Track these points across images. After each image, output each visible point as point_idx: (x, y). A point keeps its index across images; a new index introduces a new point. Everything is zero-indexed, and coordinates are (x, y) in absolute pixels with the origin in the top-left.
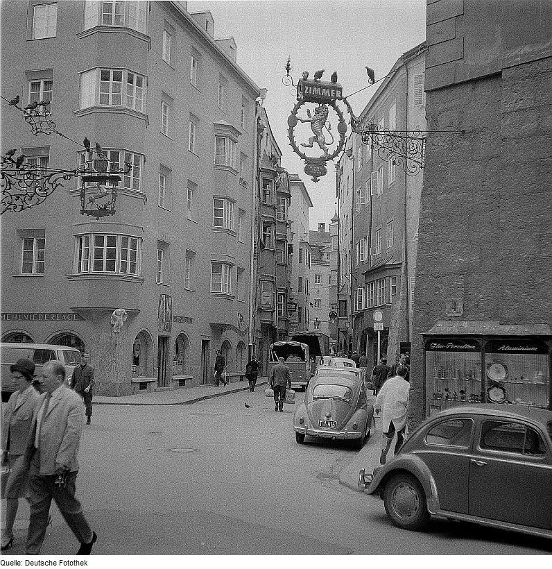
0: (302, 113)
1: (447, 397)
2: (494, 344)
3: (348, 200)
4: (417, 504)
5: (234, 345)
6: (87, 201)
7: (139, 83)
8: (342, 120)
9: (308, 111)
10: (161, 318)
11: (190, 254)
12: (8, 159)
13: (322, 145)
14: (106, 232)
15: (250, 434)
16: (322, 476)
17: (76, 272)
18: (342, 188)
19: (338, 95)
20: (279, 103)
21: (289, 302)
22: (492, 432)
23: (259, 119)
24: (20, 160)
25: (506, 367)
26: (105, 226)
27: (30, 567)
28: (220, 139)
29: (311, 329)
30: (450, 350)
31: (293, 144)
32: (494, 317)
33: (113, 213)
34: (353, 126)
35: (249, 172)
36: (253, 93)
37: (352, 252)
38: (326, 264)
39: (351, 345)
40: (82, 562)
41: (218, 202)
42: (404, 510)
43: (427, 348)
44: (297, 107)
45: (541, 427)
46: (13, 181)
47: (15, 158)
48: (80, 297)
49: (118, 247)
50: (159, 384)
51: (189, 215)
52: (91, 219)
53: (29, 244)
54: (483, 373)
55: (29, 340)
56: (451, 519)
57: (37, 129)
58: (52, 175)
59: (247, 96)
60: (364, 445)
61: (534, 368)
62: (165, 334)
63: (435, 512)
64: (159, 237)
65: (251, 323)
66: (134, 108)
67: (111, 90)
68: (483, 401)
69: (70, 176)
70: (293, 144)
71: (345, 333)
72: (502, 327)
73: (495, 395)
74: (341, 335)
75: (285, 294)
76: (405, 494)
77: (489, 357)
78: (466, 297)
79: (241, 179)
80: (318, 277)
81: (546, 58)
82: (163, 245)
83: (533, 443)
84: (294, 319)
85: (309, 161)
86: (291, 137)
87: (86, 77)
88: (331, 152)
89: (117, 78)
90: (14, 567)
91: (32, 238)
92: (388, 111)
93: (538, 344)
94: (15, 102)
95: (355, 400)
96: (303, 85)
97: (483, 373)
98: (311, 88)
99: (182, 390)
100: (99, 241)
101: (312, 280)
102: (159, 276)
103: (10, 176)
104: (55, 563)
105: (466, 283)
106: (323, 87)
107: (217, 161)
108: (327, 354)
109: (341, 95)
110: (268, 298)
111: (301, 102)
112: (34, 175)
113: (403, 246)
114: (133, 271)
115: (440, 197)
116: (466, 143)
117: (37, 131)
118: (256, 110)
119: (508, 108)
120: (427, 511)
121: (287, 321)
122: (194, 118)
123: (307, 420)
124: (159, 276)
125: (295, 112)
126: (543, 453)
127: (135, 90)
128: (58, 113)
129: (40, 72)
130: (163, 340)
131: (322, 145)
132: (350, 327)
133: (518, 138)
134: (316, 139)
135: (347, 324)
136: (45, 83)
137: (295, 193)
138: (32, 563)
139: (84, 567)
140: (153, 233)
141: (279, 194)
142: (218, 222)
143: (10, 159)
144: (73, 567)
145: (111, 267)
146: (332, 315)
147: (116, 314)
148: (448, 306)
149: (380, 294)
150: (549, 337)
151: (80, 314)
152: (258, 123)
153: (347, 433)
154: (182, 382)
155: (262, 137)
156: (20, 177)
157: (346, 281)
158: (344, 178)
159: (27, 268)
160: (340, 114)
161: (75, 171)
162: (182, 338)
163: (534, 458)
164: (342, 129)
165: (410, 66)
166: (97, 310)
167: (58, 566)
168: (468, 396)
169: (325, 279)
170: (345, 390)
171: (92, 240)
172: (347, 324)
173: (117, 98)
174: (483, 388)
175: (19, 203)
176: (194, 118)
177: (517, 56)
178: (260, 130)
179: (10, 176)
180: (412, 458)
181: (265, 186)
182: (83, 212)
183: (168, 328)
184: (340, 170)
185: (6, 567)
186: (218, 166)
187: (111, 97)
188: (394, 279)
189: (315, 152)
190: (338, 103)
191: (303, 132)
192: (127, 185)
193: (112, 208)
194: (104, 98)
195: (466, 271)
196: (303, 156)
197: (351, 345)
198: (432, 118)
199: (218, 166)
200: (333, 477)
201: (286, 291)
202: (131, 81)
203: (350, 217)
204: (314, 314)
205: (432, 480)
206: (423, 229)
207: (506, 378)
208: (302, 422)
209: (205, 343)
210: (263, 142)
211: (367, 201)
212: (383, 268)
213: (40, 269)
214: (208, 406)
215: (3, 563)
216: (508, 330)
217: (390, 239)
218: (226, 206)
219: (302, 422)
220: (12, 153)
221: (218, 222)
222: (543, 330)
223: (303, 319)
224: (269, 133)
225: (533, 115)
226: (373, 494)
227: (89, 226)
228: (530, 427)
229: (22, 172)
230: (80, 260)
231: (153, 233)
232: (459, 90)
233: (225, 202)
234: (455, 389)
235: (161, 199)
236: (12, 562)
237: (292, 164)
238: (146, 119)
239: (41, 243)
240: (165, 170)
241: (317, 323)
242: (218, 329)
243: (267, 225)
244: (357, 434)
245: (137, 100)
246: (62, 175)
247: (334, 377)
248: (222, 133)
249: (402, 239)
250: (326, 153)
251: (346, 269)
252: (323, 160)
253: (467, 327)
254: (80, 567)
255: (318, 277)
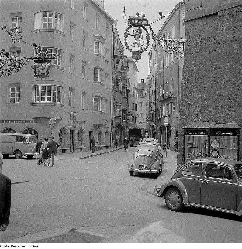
0: (130, 32)
1: (194, 155)
2: (214, 132)
3: (154, 69)
4: (179, 200)
5: (104, 133)
6: (37, 71)
7: (60, 18)
8: (148, 34)
9: (133, 30)
10: (71, 121)
11: (84, 94)
12: (2, 53)
13: (139, 45)
14: (47, 84)
15: (111, 173)
16: (140, 189)
17: (34, 102)
18: (151, 64)
19: (146, 23)
20: (122, 26)
21: (128, 114)
22: (211, 170)
23: (114, 33)
24: (8, 53)
25: (219, 142)
26: (45, 82)
27: (13, 248)
28: (96, 43)
29: (138, 126)
30: (195, 134)
31: (126, 45)
32: (214, 120)
33: (48, 76)
34: (153, 37)
35: (109, 57)
36: (111, 21)
37: (156, 92)
38: (144, 97)
39: (155, 133)
40: (36, 246)
41: (96, 70)
42: (173, 203)
43: (185, 134)
44: (128, 29)
45: (232, 167)
46: (4, 62)
47: (5, 53)
48: (35, 113)
49: (52, 91)
50: (71, 150)
51: (83, 77)
52: (39, 79)
53: (13, 89)
54: (209, 144)
55: (14, 132)
56: (193, 206)
57: (14, 40)
58: (21, 60)
59: (108, 23)
60: (159, 175)
61: (231, 142)
62: (73, 129)
63: (187, 204)
64: (70, 86)
65: (111, 124)
66: (58, 29)
67: (48, 21)
68: (209, 157)
69: (29, 60)
70: (126, 45)
71: (153, 127)
72: (217, 125)
73: (214, 154)
74: (151, 128)
75: (126, 110)
76: (174, 196)
77: (212, 138)
78: (202, 112)
79: (106, 60)
80: (141, 103)
81: (238, 6)
82: (72, 90)
83: (229, 174)
84: (130, 121)
85: (133, 53)
86: (126, 42)
87: (37, 15)
88: (143, 49)
89: (50, 16)
90: (6, 248)
91: (14, 88)
92: (171, 30)
93: (234, 132)
94: (4, 28)
95: (156, 156)
96: (130, 19)
97: (209, 144)
98: (134, 20)
99: (81, 153)
100: (43, 88)
101: (138, 104)
102: (70, 103)
103: (3, 60)
104: (24, 246)
105: (202, 106)
106: (139, 20)
107: (95, 52)
108: (145, 137)
109: (148, 23)
110: (118, 112)
111: (130, 26)
112: (13, 60)
113: (178, 89)
114: (58, 101)
115: (191, 68)
116: (202, 44)
117: (14, 41)
118: (113, 29)
119: (221, 28)
120: (184, 204)
121: (127, 122)
122: (85, 33)
123: (134, 165)
124: (70, 103)
125: (127, 31)
126: (232, 178)
127: (58, 21)
128: (25, 32)
129: (16, 13)
130: (72, 131)
131: (139, 45)
132: (155, 125)
133: (225, 42)
134: (136, 43)
135: (153, 124)
136: (19, 18)
137: (131, 66)
138: (14, 246)
139: (37, 248)
140: (67, 85)
141: (123, 66)
142: (96, 79)
143: (3, 53)
144: (32, 248)
145: (49, 99)
146: (147, 120)
147: (52, 120)
148: (194, 116)
149: (167, 110)
150: (239, 129)
151: (36, 120)
152: (114, 35)
153: (152, 171)
154: (81, 149)
155: (115, 41)
156: (8, 61)
157: (153, 105)
158: (152, 59)
159: (13, 100)
160: (147, 32)
161: (31, 58)
162: (81, 130)
163: (229, 180)
164: (148, 39)
165: (181, 9)
166: (43, 118)
167: (25, 248)
168: (203, 155)
169: (144, 104)
170: (151, 152)
171: (41, 88)
172: (153, 124)
173: (50, 25)
174: (209, 151)
175: (7, 72)
176: (85, 33)
177: (225, 5)
178: (114, 38)
179: (3, 60)
180: (179, 182)
181: (117, 63)
182: (35, 76)
183: (74, 126)
184: (150, 55)
185: (2, 248)
186: (97, 55)
187: (48, 24)
188: (174, 104)
189: (136, 49)
190: (146, 27)
191: (131, 40)
192: (55, 63)
193: (48, 74)
194: (45, 25)
195: (202, 100)
196: (131, 50)
197: (155, 133)
198: (188, 33)
199: (97, 55)
200: (145, 189)
201: (127, 109)
202: (56, 17)
203: (154, 76)
204: (139, 119)
205: (185, 190)
206: (183, 83)
207: (219, 146)
208: (132, 166)
209: (91, 132)
210: (116, 43)
211: (162, 69)
212: (168, 99)
213: (18, 100)
214: (90, 160)
215: (1, 246)
216: (220, 126)
217: (172, 86)
218: (99, 72)
219: (132, 166)
220: (4, 50)
221: (96, 79)
222: (235, 126)
223: (134, 122)
224: (119, 40)
225: (232, 32)
226: (160, 196)
227: (38, 82)
228: (228, 168)
229: (8, 59)
230: (36, 97)
231: (67, 85)
232: (200, 20)
233: (99, 70)
234: (197, 151)
235: (71, 70)
236: (5, 246)
237: (128, 54)
238: (63, 34)
239: (18, 89)
240: (72, 57)
241: (141, 123)
242: (97, 126)
243: (118, 80)
244: (156, 171)
245: (59, 25)
246: (26, 60)
247: (147, 146)
248: (97, 40)
249: (172, 88)
250: (141, 49)
251: (153, 100)
252: (140, 52)
253: (202, 125)
254: (35, 248)
255: (141, 103)
